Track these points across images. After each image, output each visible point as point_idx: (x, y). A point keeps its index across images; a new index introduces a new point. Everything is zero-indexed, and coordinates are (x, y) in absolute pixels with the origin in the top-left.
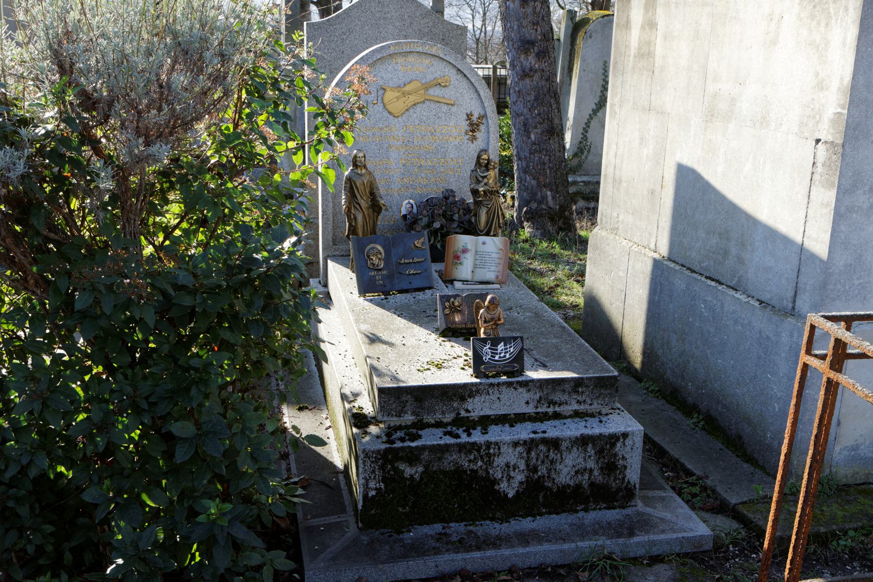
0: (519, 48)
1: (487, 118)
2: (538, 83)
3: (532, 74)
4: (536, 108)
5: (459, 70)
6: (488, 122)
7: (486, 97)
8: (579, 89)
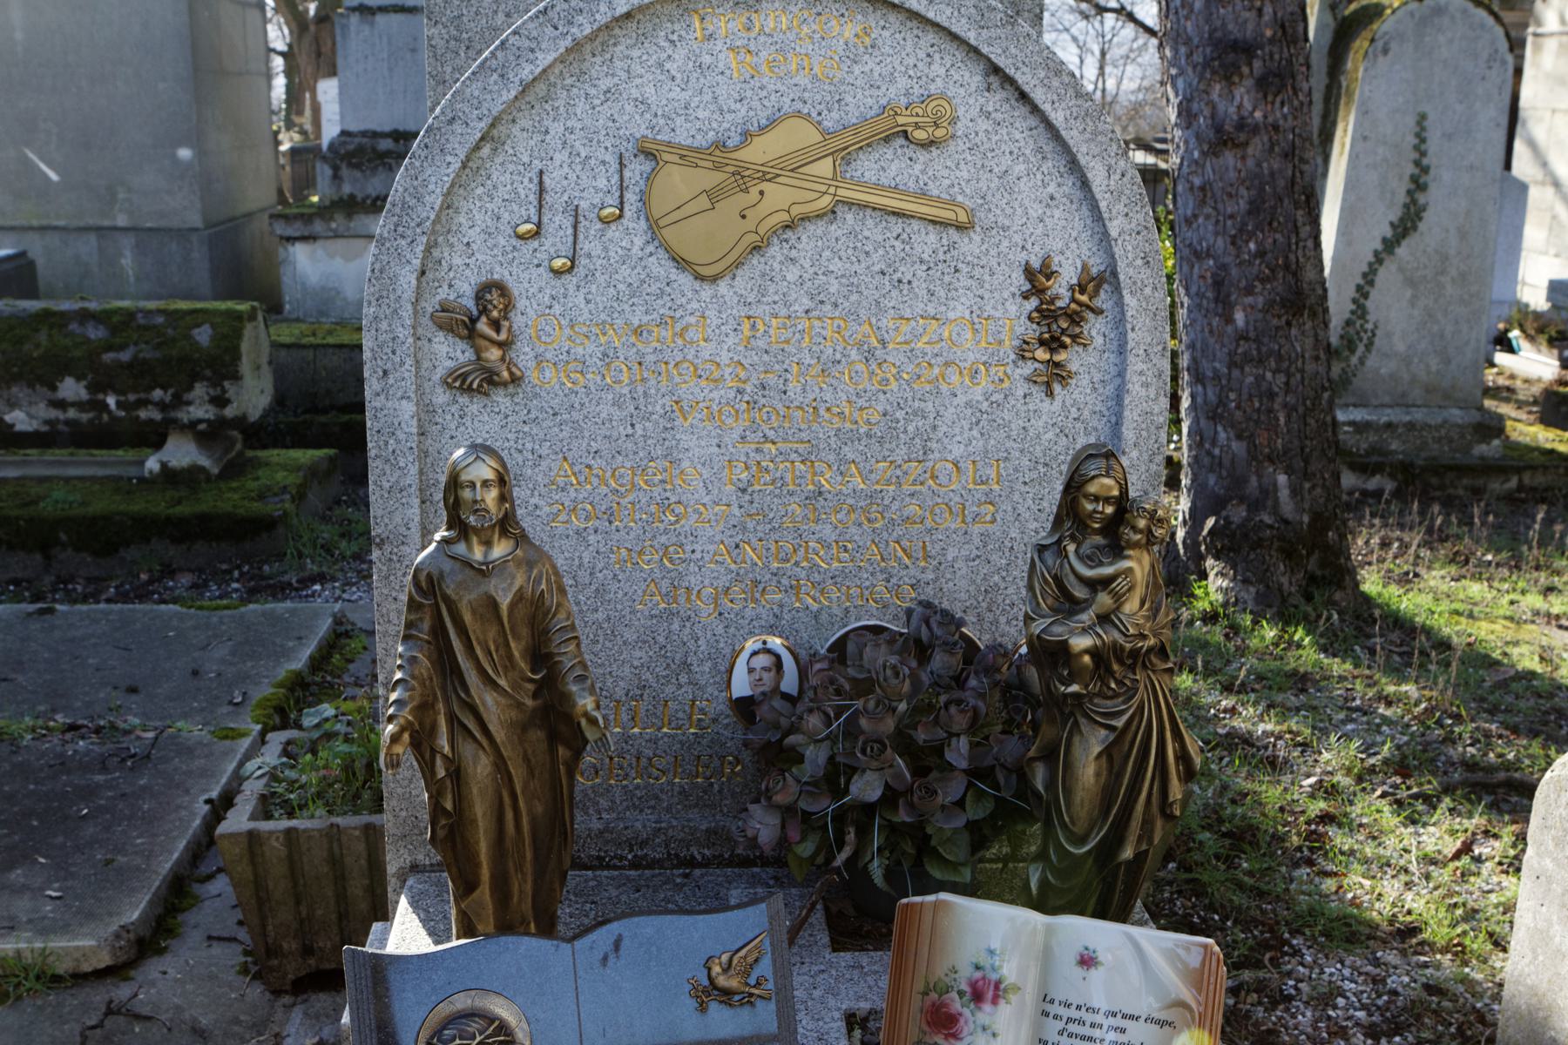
0: (1206, 64)
1: (1117, 289)
2: (1259, 165)
3: (1242, 137)
4: (1251, 235)
5: (996, 70)
6: (1120, 303)
7: (1117, 195)
8: (1351, 185)
